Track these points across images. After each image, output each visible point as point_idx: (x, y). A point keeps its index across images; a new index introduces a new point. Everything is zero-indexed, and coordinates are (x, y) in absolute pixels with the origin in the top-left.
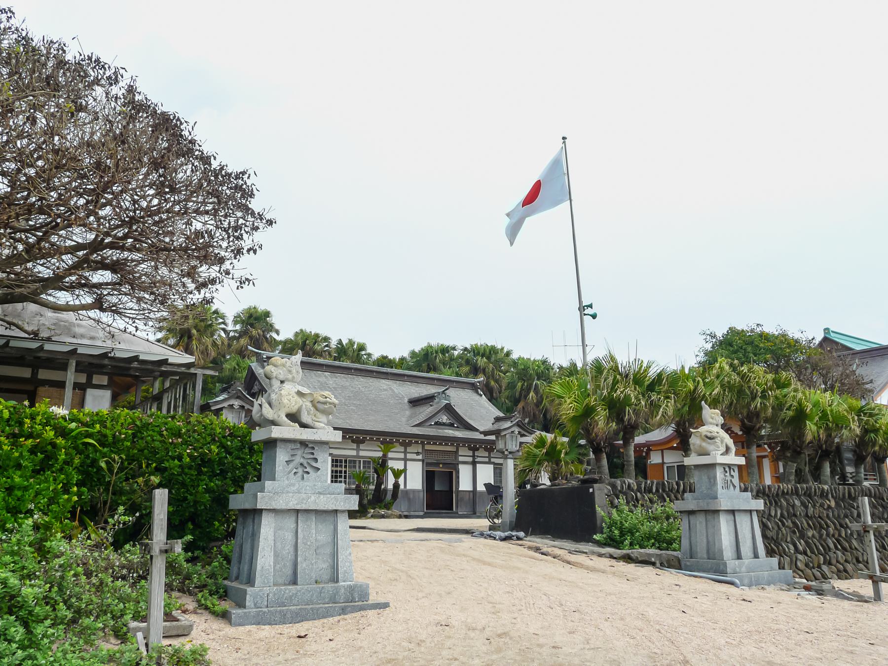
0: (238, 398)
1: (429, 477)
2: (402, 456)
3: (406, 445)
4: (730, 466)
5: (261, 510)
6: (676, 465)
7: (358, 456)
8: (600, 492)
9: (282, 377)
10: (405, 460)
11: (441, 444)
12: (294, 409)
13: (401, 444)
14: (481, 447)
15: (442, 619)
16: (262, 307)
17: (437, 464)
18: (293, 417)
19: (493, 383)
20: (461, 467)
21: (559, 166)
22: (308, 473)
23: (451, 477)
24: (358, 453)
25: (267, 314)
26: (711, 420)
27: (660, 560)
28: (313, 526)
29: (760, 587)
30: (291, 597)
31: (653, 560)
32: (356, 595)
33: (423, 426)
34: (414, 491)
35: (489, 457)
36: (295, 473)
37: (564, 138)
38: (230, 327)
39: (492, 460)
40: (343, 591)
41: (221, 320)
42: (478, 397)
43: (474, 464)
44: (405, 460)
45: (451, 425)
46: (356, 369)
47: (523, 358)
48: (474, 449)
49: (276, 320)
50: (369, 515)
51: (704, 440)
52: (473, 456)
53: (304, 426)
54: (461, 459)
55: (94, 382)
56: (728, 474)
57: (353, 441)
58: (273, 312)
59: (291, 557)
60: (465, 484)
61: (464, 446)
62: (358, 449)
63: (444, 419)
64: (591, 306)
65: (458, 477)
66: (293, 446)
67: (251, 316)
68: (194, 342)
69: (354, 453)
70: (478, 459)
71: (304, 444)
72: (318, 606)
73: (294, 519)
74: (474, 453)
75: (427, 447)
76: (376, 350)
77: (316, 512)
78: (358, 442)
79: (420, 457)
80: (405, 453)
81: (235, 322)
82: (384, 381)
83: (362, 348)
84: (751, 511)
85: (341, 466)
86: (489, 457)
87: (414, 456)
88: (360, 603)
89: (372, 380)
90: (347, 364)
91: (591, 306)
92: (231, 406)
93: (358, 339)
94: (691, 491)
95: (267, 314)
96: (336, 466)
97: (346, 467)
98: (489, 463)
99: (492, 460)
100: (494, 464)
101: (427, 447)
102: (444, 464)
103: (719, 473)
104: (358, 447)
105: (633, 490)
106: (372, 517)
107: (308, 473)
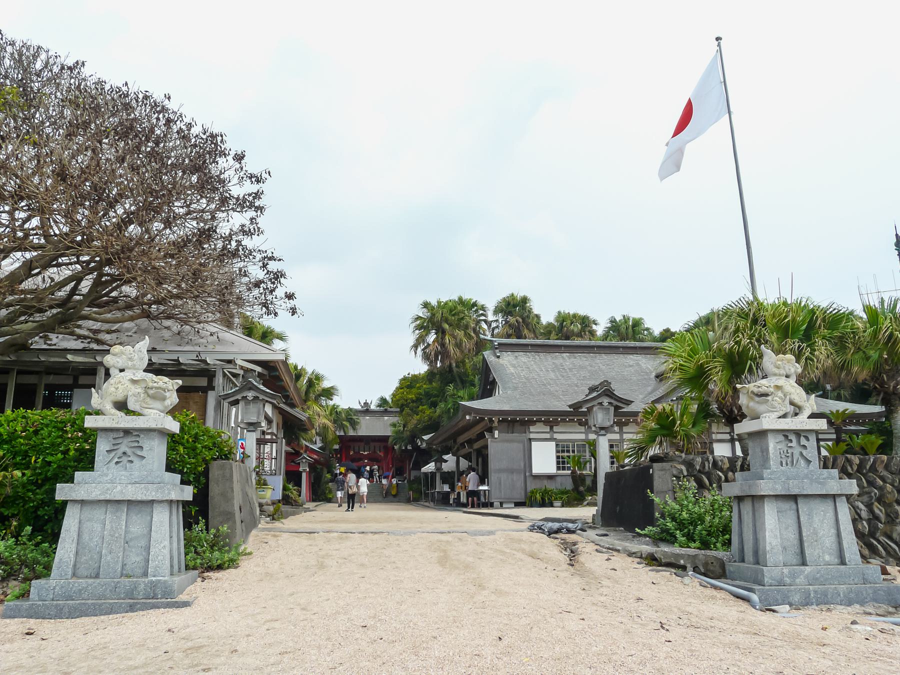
0: (250, 389)
2: (727, 437)
4: (798, 433)
5: (763, 497)
8: (661, 476)
9: (120, 365)
12: (120, 397)
16: (520, 294)
18: (122, 406)
21: (718, 75)
22: (131, 462)
24: (621, 436)
25: (525, 300)
26: (776, 371)
27: (693, 562)
28: (124, 517)
29: (824, 607)
30: (80, 590)
31: (682, 562)
36: (117, 463)
37: (718, 39)
38: (491, 317)
39: (556, 436)
40: (142, 586)
41: (481, 312)
49: (536, 307)
50: (585, 503)
51: (752, 399)
53: (129, 412)
56: (794, 444)
57: (580, 424)
59: (796, 542)
62: (621, 432)
66: (115, 435)
67: (508, 304)
68: (447, 337)
69: (583, 436)
71: (127, 432)
72: (100, 602)
73: (832, 504)
77: (130, 502)
81: (496, 312)
82: (631, 356)
83: (637, 323)
84: (834, 497)
85: (568, 451)
88: (163, 600)
89: (616, 356)
92: (245, 398)
93: (634, 315)
94: (742, 469)
95: (525, 300)
96: (563, 451)
97: (573, 451)
98: (551, 439)
99: (556, 436)
103: (773, 445)
105: (721, 470)
106: (588, 504)
107: (131, 462)
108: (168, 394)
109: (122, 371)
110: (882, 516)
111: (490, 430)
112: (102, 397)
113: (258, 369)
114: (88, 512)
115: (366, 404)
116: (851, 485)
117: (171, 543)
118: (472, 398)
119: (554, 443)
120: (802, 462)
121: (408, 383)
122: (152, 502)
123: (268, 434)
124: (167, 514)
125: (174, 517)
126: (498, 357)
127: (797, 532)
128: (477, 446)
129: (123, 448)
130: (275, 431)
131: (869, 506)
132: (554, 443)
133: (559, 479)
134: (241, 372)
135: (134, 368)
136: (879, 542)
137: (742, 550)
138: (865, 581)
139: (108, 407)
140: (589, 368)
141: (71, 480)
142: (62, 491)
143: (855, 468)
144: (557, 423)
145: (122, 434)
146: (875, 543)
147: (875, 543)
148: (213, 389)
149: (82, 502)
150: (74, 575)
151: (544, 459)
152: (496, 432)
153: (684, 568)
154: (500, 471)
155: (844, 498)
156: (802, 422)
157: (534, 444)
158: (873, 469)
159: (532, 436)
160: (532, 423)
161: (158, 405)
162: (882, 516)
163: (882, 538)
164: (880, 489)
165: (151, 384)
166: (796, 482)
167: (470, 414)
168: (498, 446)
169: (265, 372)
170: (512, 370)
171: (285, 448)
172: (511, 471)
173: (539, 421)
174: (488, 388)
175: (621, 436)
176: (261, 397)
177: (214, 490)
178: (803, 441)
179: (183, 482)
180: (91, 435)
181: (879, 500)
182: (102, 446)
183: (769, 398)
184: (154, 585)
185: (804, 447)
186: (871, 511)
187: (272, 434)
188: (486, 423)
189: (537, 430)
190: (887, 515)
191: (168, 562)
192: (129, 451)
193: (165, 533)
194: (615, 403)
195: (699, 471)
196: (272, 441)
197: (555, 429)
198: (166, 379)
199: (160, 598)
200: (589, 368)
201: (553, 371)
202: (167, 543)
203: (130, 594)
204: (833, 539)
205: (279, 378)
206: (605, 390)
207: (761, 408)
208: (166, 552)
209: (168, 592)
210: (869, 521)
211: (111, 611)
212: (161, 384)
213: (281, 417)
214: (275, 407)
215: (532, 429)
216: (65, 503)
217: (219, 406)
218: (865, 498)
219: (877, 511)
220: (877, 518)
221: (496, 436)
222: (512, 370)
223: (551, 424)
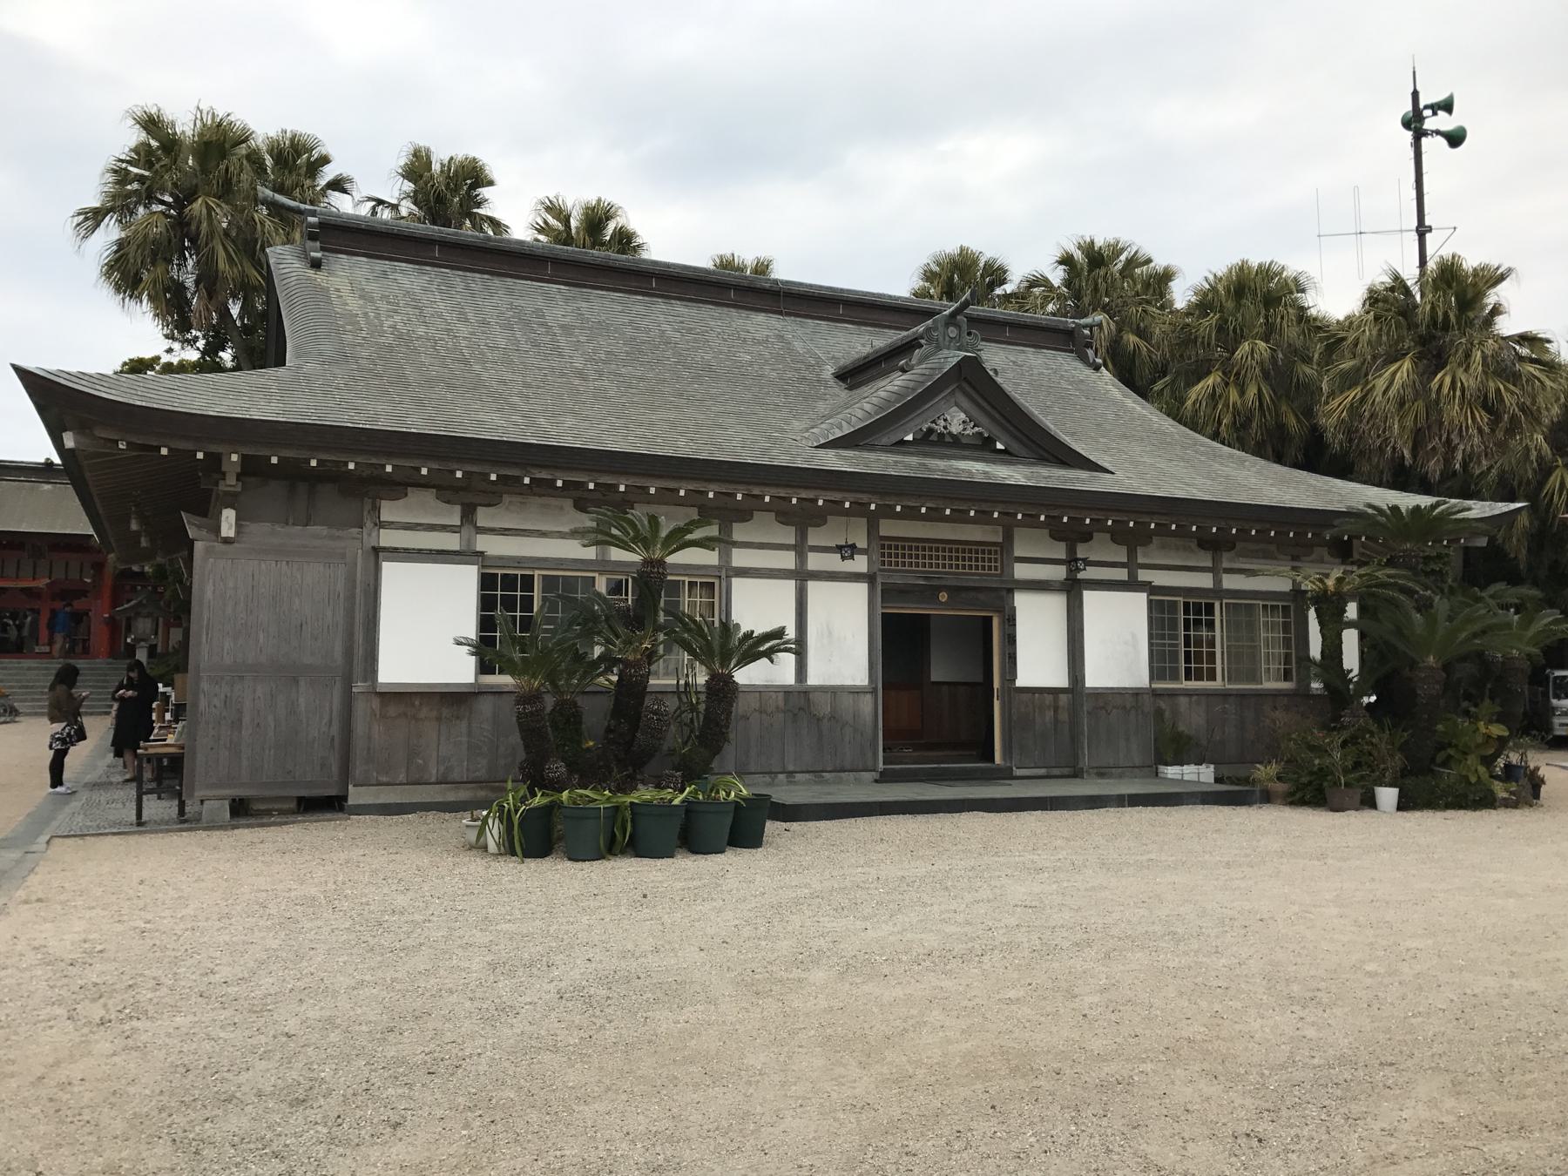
1: (899, 640)
2: (1059, 573)
3: (803, 519)
6: (687, 579)
10: (802, 576)
11: (935, 516)
13: (785, 515)
14: (1098, 524)
17: (928, 592)
19: (1132, 339)
20: (813, 679)
23: (987, 636)
33: (872, 448)
34: (834, 691)
35: (1131, 565)
42: (1089, 372)
43: (1073, 589)
44: (802, 576)
45: (983, 447)
47: (1218, 279)
48: (1073, 536)
52: (1072, 562)
54: (1022, 571)
60: (1038, 661)
61: (1031, 521)
63: (956, 421)
64: (1447, 106)
65: (1010, 640)
69: (1204, 581)
74: (1071, 550)
75: (888, 528)
76: (783, 272)
78: (1215, 545)
79: (860, 564)
80: (800, 549)
86: (1131, 565)
87: (833, 562)
91: (1447, 106)
98: (1131, 585)
99: (1144, 575)
101: (888, 528)
102: (954, 591)
111: (206, 509)
119: (1139, 600)
126: (316, 265)
132: (1139, 600)
133: (485, 706)
144: (492, 496)
151: (426, 628)
152: (228, 517)
157: (391, 572)
159: (388, 538)
160: (398, 487)
170: (354, 304)
172: (289, 674)
173: (835, 508)
189: (406, 517)
197: (484, 517)
200: (629, 331)
222: (354, 304)
223: (1132, 540)
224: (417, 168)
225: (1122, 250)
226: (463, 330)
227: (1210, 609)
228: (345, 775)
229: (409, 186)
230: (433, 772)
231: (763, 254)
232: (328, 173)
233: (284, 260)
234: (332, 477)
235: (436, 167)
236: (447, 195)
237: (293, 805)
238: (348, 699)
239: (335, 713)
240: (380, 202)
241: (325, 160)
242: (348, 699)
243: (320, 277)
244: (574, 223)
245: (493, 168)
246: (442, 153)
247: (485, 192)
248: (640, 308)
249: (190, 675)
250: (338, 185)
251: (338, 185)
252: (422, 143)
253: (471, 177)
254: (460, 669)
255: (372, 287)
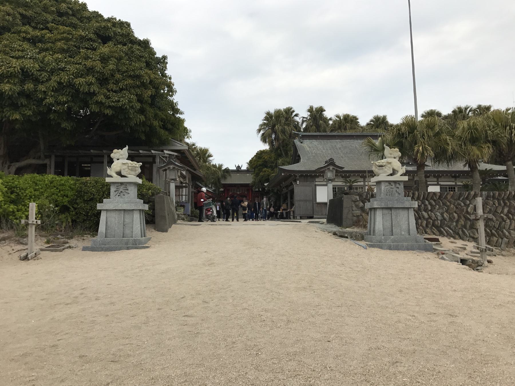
4: (395, 182)
7: (456, 185)
9: (117, 158)
15: (10, 256)
18: (119, 174)
24: (364, 183)
31: (346, 235)
32: (137, 243)
35: (438, 181)
39: (440, 183)
46: (320, 136)
55: (152, 158)
57: (342, 177)
58: (267, 110)
59: (390, 227)
69: (454, 184)
70: (428, 183)
71: (122, 183)
78: (455, 177)
84: (408, 208)
86: (438, 181)
90: (348, 133)
92: (169, 168)
98: (438, 185)
99: (440, 183)
100: (440, 185)
104: (438, 179)
108: (137, 169)
109: (118, 159)
110: (447, 218)
111: (295, 181)
112: (112, 171)
113: (176, 154)
114: (109, 214)
115: (239, 166)
116: (415, 204)
117: (141, 226)
118: (289, 164)
119: (439, 187)
120: (397, 194)
121: (260, 155)
122: (133, 210)
123: (184, 183)
124: (139, 215)
125: (142, 216)
126: (302, 143)
127: (391, 223)
128: (290, 189)
129: (121, 190)
130: (187, 182)
131: (442, 214)
132: (439, 187)
134: (168, 156)
135: (123, 158)
136: (445, 230)
137: (370, 231)
138: (417, 242)
139: (114, 175)
140: (350, 147)
141: (102, 202)
142: (99, 206)
143: (438, 197)
145: (120, 184)
146: (442, 230)
147: (442, 230)
148: (155, 163)
149: (107, 210)
150: (106, 237)
152: (298, 182)
153: (347, 237)
154: (300, 201)
155: (412, 209)
156: (397, 177)
157: (318, 188)
158: (446, 198)
159: (317, 183)
161: (133, 173)
162: (447, 218)
163: (446, 228)
164: (448, 206)
165: (130, 165)
166: (391, 202)
167: (284, 173)
168: (300, 189)
169: (179, 155)
171: (191, 190)
172: (306, 201)
174: (296, 159)
175: (364, 183)
176: (176, 168)
177: (157, 207)
178: (398, 185)
179: (144, 203)
180: (109, 185)
181: (447, 211)
182: (113, 189)
183: (384, 167)
184: (135, 241)
185: (398, 188)
186: (443, 216)
187: (186, 183)
188: (293, 176)
190: (450, 218)
191: (140, 232)
192: (123, 191)
193: (137, 222)
194: (336, 168)
195: (365, 199)
196: (186, 187)
198: (136, 163)
199: (137, 245)
201: (331, 149)
202: (139, 225)
203: (127, 243)
204: (407, 225)
205: (186, 157)
206: (331, 163)
207: (381, 171)
208: (139, 228)
209: (140, 243)
210: (441, 221)
211: (120, 249)
212: (134, 165)
213: (190, 175)
214: (188, 170)
215: (317, 180)
216: (101, 211)
217: (158, 171)
218: (441, 211)
219: (445, 216)
220: (445, 219)
221: (298, 183)
222: (308, 149)
224: (311, 110)
225: (468, 108)
226: (324, 151)
227: (454, 188)
228: (313, 213)
229: (309, 113)
230: (324, 214)
231: (385, 114)
232: (294, 114)
233: (297, 141)
234: (311, 176)
235: (314, 109)
236: (317, 115)
237: (375, 184)
238: (313, 203)
239: (49, 245)
240: (304, 117)
241: (293, 111)
242: (313, 203)
243: (302, 144)
244: (342, 118)
245: (325, 108)
246: (316, 106)
247: (324, 113)
248: (352, 142)
249: (193, 202)
250: (296, 115)
251: (296, 115)
252: (311, 105)
253: (321, 110)
254: (106, 181)
255: (310, 145)
